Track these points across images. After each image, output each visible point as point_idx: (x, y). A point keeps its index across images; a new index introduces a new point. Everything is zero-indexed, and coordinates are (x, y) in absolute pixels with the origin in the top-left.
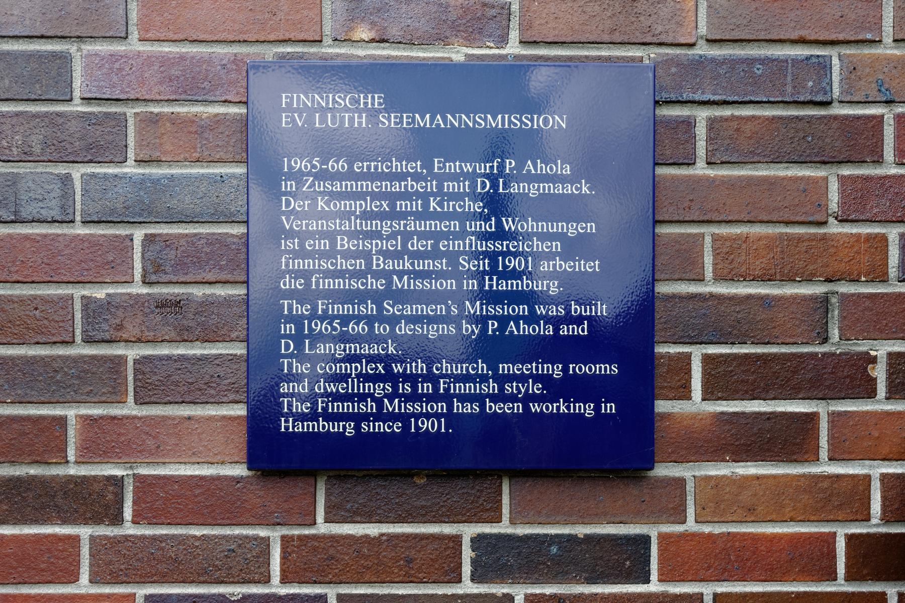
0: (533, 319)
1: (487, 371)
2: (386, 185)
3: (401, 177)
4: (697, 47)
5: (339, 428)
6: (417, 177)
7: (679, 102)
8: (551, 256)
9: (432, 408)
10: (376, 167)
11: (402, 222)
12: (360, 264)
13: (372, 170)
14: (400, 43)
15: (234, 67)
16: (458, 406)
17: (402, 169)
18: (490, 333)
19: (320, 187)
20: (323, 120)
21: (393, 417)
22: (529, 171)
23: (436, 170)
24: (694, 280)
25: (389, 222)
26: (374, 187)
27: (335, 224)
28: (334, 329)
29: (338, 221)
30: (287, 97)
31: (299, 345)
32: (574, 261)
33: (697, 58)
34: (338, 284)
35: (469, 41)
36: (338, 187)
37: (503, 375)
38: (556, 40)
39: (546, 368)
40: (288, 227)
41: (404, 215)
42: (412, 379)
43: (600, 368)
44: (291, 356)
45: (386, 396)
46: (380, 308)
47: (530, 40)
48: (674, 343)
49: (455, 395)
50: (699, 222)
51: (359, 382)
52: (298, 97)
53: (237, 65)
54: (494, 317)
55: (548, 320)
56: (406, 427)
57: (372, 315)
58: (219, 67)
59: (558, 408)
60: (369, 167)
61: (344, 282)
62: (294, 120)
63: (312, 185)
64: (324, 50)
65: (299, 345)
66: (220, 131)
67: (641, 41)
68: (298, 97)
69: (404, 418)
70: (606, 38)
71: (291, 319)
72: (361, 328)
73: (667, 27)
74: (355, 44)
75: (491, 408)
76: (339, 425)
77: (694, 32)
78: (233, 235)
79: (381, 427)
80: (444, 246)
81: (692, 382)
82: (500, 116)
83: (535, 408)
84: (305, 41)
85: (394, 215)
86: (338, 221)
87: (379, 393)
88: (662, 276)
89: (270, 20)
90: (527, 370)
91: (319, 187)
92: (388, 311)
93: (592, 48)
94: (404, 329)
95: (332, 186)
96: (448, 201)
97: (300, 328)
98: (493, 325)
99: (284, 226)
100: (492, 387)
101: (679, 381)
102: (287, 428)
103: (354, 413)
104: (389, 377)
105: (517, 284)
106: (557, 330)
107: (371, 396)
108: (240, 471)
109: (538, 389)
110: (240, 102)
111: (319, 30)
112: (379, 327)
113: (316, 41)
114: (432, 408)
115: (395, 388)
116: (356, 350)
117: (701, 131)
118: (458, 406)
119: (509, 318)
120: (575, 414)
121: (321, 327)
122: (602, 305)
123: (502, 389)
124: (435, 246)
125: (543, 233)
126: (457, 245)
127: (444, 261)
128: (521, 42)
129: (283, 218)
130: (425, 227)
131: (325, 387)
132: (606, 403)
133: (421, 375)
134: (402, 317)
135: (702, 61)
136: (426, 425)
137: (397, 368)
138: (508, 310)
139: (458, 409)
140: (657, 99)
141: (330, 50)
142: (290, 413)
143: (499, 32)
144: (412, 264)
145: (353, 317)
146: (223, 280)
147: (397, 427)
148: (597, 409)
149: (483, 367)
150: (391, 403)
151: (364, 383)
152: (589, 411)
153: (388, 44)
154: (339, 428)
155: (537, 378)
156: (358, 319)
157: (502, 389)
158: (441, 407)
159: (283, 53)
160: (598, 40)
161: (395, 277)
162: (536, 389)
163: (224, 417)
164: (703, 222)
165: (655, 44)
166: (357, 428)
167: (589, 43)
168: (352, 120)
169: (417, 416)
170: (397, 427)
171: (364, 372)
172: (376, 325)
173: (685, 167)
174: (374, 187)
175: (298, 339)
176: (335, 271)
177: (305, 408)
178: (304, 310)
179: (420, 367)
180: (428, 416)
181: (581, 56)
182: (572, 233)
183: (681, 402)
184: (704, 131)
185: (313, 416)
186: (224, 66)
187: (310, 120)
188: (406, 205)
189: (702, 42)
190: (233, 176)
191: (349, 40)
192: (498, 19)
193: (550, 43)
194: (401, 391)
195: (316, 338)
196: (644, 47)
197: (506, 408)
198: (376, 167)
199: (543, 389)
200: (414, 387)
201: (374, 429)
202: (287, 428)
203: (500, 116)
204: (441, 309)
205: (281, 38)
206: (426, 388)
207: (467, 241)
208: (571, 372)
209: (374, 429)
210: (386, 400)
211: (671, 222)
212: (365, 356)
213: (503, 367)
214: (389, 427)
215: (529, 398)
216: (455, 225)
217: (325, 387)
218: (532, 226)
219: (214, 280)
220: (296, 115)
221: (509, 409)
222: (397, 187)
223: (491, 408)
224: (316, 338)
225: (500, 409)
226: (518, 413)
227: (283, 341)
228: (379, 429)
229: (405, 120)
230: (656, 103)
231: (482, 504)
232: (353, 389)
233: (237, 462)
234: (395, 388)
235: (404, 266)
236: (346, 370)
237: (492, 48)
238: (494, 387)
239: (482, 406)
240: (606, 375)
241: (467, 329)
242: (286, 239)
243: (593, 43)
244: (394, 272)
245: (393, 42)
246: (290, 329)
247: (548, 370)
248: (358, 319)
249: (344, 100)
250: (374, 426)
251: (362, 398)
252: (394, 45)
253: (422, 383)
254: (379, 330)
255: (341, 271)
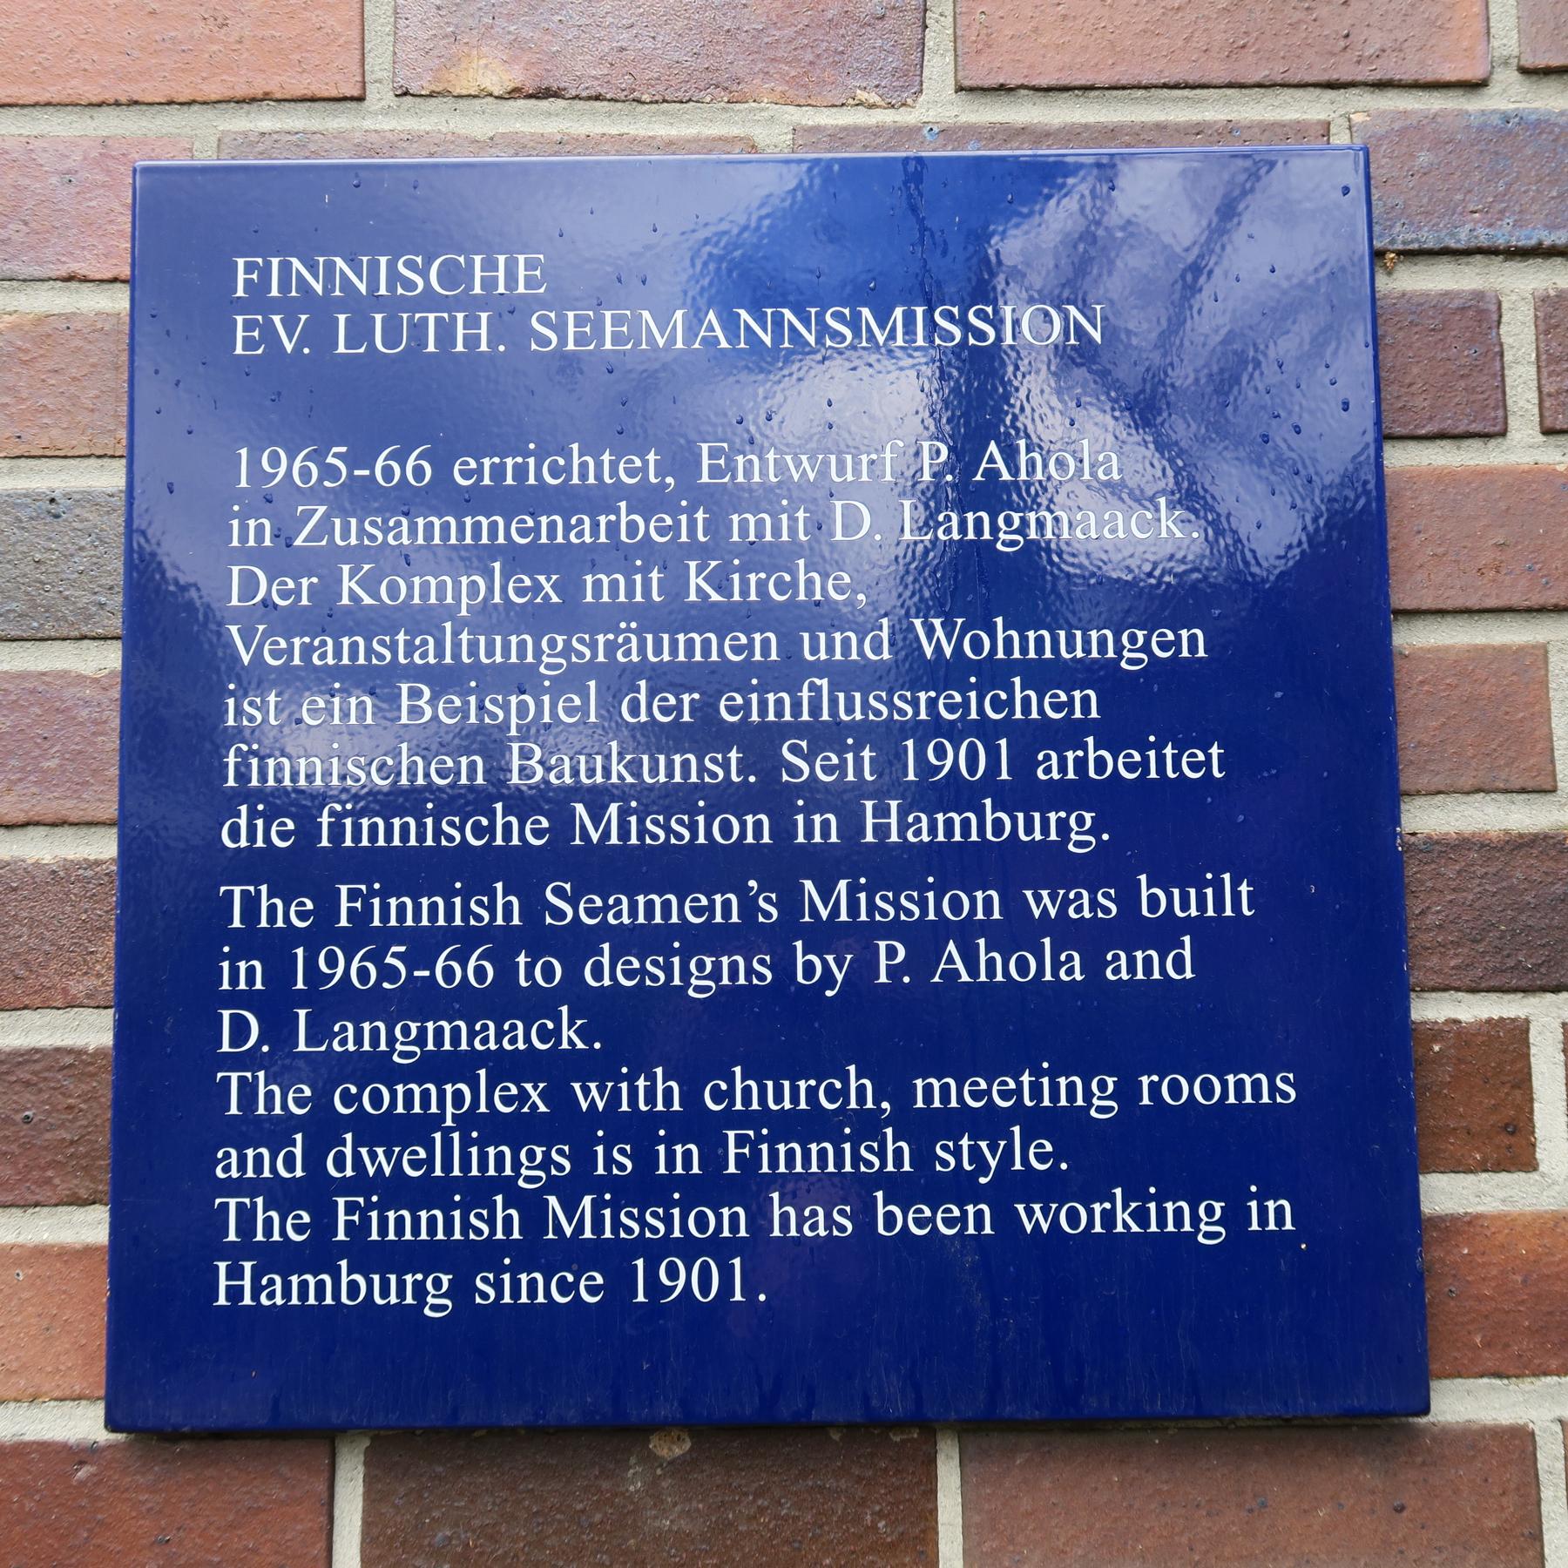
0: (1016, 932)
1: (876, 1101)
2: (552, 526)
3: (598, 500)
4: (1494, 89)
5: (401, 1293)
6: (648, 501)
7: (1446, 252)
8: (1067, 735)
9: (702, 1222)
10: (520, 472)
11: (601, 638)
12: (471, 770)
13: (509, 481)
14: (597, 98)
15: (101, 178)
16: (785, 1217)
17: (599, 476)
18: (883, 979)
19: (348, 533)
20: (360, 332)
21: (576, 1254)
22: (992, 474)
23: (705, 479)
24: (1523, 791)
25: (560, 639)
26: (512, 531)
27: (393, 647)
28: (388, 973)
29: (401, 637)
30: (249, 268)
31: (278, 1029)
32: (1143, 748)
33: (1496, 120)
34: (402, 832)
35: (802, 92)
36: (403, 533)
37: (928, 1111)
38: (1066, 80)
39: (1067, 1091)
40: (246, 659)
41: (605, 618)
42: (639, 1131)
43: (1240, 1085)
44: (249, 1061)
45: (553, 1186)
46: (534, 907)
47: (987, 83)
48: (1473, 990)
49: (774, 1180)
50: (1529, 610)
51: (466, 1143)
52: (285, 268)
53: (108, 172)
54: (894, 930)
55: (1067, 933)
56: (620, 1282)
57: (508, 929)
58: (54, 180)
59: (1109, 1218)
60: (498, 472)
61: (421, 827)
62: (269, 331)
63: (325, 527)
64: (369, 124)
65: (278, 1029)
66: (51, 365)
67: (1324, 78)
68: (285, 268)
69: (612, 1257)
70: (1219, 73)
71: (252, 942)
72: (476, 969)
73: (1401, 36)
74: (462, 104)
75: (890, 1219)
76: (401, 1285)
77: (1481, 48)
78: (81, 679)
79: (539, 1288)
80: (732, 710)
81: (1537, 1116)
82: (898, 312)
83: (1033, 1218)
84: (313, 100)
85: (570, 616)
86: (401, 637)
87: (529, 1176)
88: (1423, 781)
89: (211, 40)
90: (1005, 1095)
91: (345, 535)
92: (559, 914)
93: (1174, 100)
94: (607, 971)
95: (386, 531)
96: (744, 570)
97: (280, 972)
98: (889, 955)
99: (238, 658)
100: (894, 1152)
101: (1495, 1109)
102: (235, 1293)
103: (448, 1244)
104: (565, 1124)
105: (966, 824)
106: (1094, 966)
107: (507, 1186)
108: (84, 1424)
109: (1041, 1158)
110: (115, 280)
111: (356, 69)
112: (530, 968)
113: (345, 99)
114: (702, 1222)
115: (583, 1159)
116: (456, 1040)
117: (1519, 337)
118: (785, 1217)
119: (941, 930)
120: (1162, 1235)
121: (347, 968)
122: (1235, 884)
123: (923, 1157)
124: (706, 711)
125: (1041, 661)
126: (774, 706)
127: (734, 755)
128: (960, 89)
129: (234, 629)
130: (674, 651)
131: (357, 1157)
132: (1261, 1198)
133: (667, 1118)
134: (604, 931)
135: (1512, 128)
136: (683, 1279)
137: (590, 1096)
138: (937, 907)
139: (785, 1226)
140: (1377, 244)
141: (387, 124)
142: (246, 1247)
143: (893, 62)
144: (635, 768)
145: (450, 934)
146: (50, 818)
147: (589, 1288)
148: (1235, 1218)
149: (861, 1090)
150: (570, 1208)
151: (482, 1144)
152: (1208, 1225)
153: (561, 103)
154: (401, 1293)
155: (1037, 1122)
156: (465, 940)
157: (923, 1157)
158: (730, 1220)
159: (245, 134)
160: (1191, 79)
161: (580, 809)
162: (1035, 1156)
163: (41, 1252)
164: (1542, 610)
165: (1366, 84)
166: (462, 1291)
167: (1165, 86)
168: (446, 332)
169: (655, 1251)
170: (589, 1288)
171: (483, 1109)
172: (522, 959)
173: (1476, 444)
174: (512, 531)
175: (274, 1006)
176: (396, 790)
177: (292, 1228)
178: (294, 914)
179: (660, 1090)
180: (689, 1249)
181: (1143, 126)
182: (1131, 660)
183: (1504, 1176)
184: (1529, 334)
185: (319, 1254)
186: (68, 177)
187: (320, 334)
188: (614, 585)
189: (1507, 78)
190: (87, 499)
191: (445, 93)
192: (888, 24)
193: (1049, 89)
194: (601, 1171)
195: (336, 1004)
196: (1330, 94)
197: (943, 1221)
198: (520, 472)
199: (1057, 1156)
200: (645, 1159)
201: (515, 1293)
202: (235, 1293)
203: (898, 312)
204: (725, 906)
205: (240, 92)
206: (684, 1158)
207: (805, 694)
208: (1146, 1101)
209: (515, 1293)
210: (553, 1201)
211: (1441, 612)
212: (484, 1058)
213: (928, 1090)
214: (564, 1288)
215: (1013, 1188)
216: (765, 645)
217: (357, 1157)
218: (1008, 641)
219: (22, 818)
220: (277, 319)
221: (949, 1223)
222: (584, 531)
223: (890, 1219)
224: (336, 1004)
225: (920, 1223)
226: (978, 1238)
227: (226, 1014)
228: (532, 1292)
229: (609, 329)
230: (1377, 255)
231: (874, 1527)
232: (448, 1166)
233: (79, 1398)
234: (583, 1159)
235: (607, 772)
236: (425, 1102)
237: (872, 106)
238: (898, 1153)
239: (864, 1216)
240: (1257, 1107)
241: (809, 969)
242: (239, 697)
243: (1176, 86)
244: (577, 792)
245: (577, 97)
246: (250, 973)
247: (1071, 1095)
248: (465, 940)
249: (424, 274)
250: (516, 1285)
251: (478, 1192)
252: (580, 104)
253: (670, 1142)
254: (530, 975)
255: (413, 790)
